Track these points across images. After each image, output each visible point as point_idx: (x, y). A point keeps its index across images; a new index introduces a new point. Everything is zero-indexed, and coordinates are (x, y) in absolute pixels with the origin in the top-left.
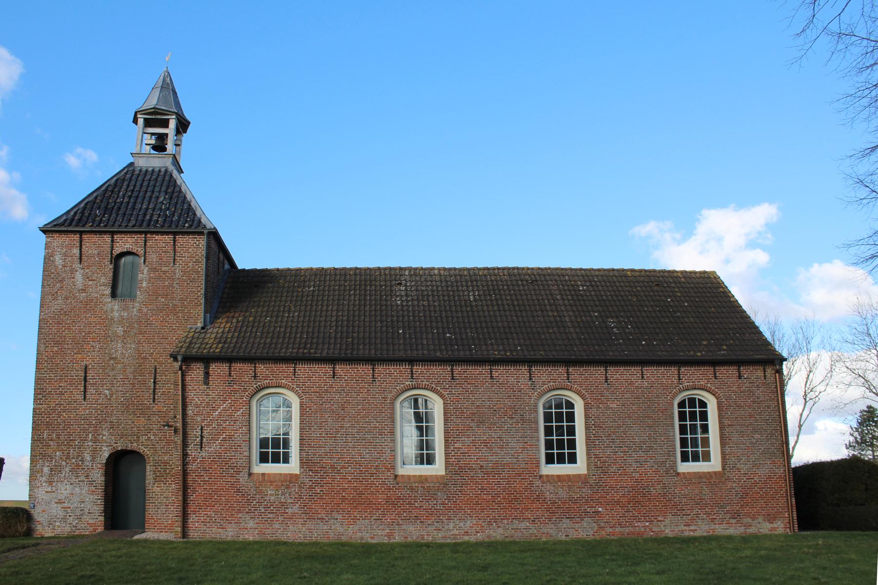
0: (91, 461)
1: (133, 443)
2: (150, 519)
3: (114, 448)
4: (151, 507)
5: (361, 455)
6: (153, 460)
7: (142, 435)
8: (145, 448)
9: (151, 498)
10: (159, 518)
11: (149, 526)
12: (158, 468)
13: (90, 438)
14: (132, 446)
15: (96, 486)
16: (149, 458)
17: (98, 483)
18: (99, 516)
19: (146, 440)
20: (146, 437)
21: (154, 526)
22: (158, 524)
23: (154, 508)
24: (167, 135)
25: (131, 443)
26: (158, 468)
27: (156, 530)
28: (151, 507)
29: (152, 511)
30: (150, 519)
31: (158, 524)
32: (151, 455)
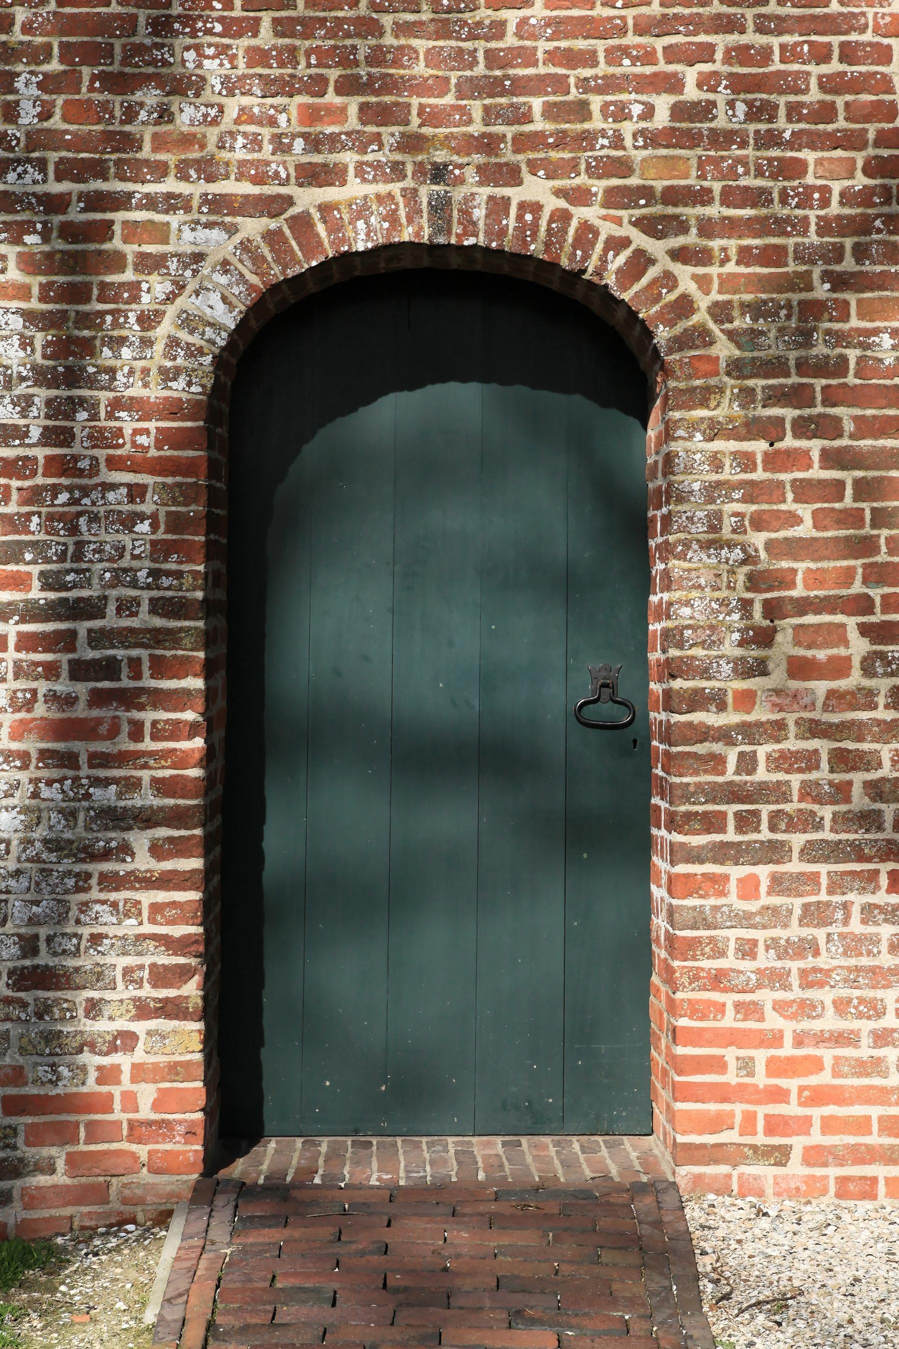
0: (42, 377)
1: (513, 176)
2: (732, 1038)
3: (302, 223)
4: (733, 900)
5: (346, 59)
6: (736, 368)
7: (609, 85)
8: (648, 226)
9: (734, 793)
10: (830, 1022)
11: (718, 1123)
12: (799, 459)
13: (28, 115)
14: (498, 206)
15: (110, 669)
16: (703, 337)
17: (127, 637)
18: (143, 1011)
19: (652, 139)
20: (663, 103)
21: (774, 1125)
22: (818, 1096)
23: (776, 916)
24: (767, 1116)
25: (489, 175)
26: (799, 459)
27: (796, 1167)
28: (733, 900)
29: (748, 950)
30: (732, 1038)
31: (818, 1096)
32: (721, 312)
